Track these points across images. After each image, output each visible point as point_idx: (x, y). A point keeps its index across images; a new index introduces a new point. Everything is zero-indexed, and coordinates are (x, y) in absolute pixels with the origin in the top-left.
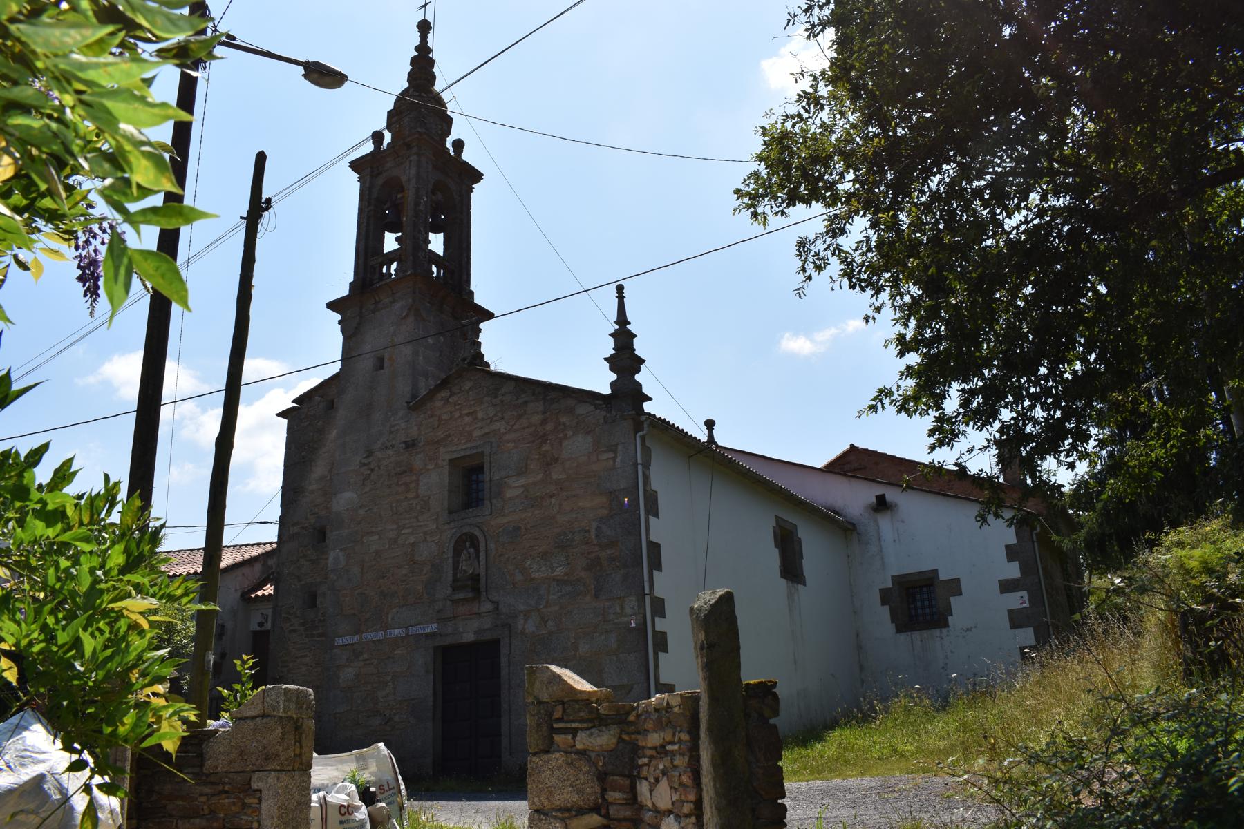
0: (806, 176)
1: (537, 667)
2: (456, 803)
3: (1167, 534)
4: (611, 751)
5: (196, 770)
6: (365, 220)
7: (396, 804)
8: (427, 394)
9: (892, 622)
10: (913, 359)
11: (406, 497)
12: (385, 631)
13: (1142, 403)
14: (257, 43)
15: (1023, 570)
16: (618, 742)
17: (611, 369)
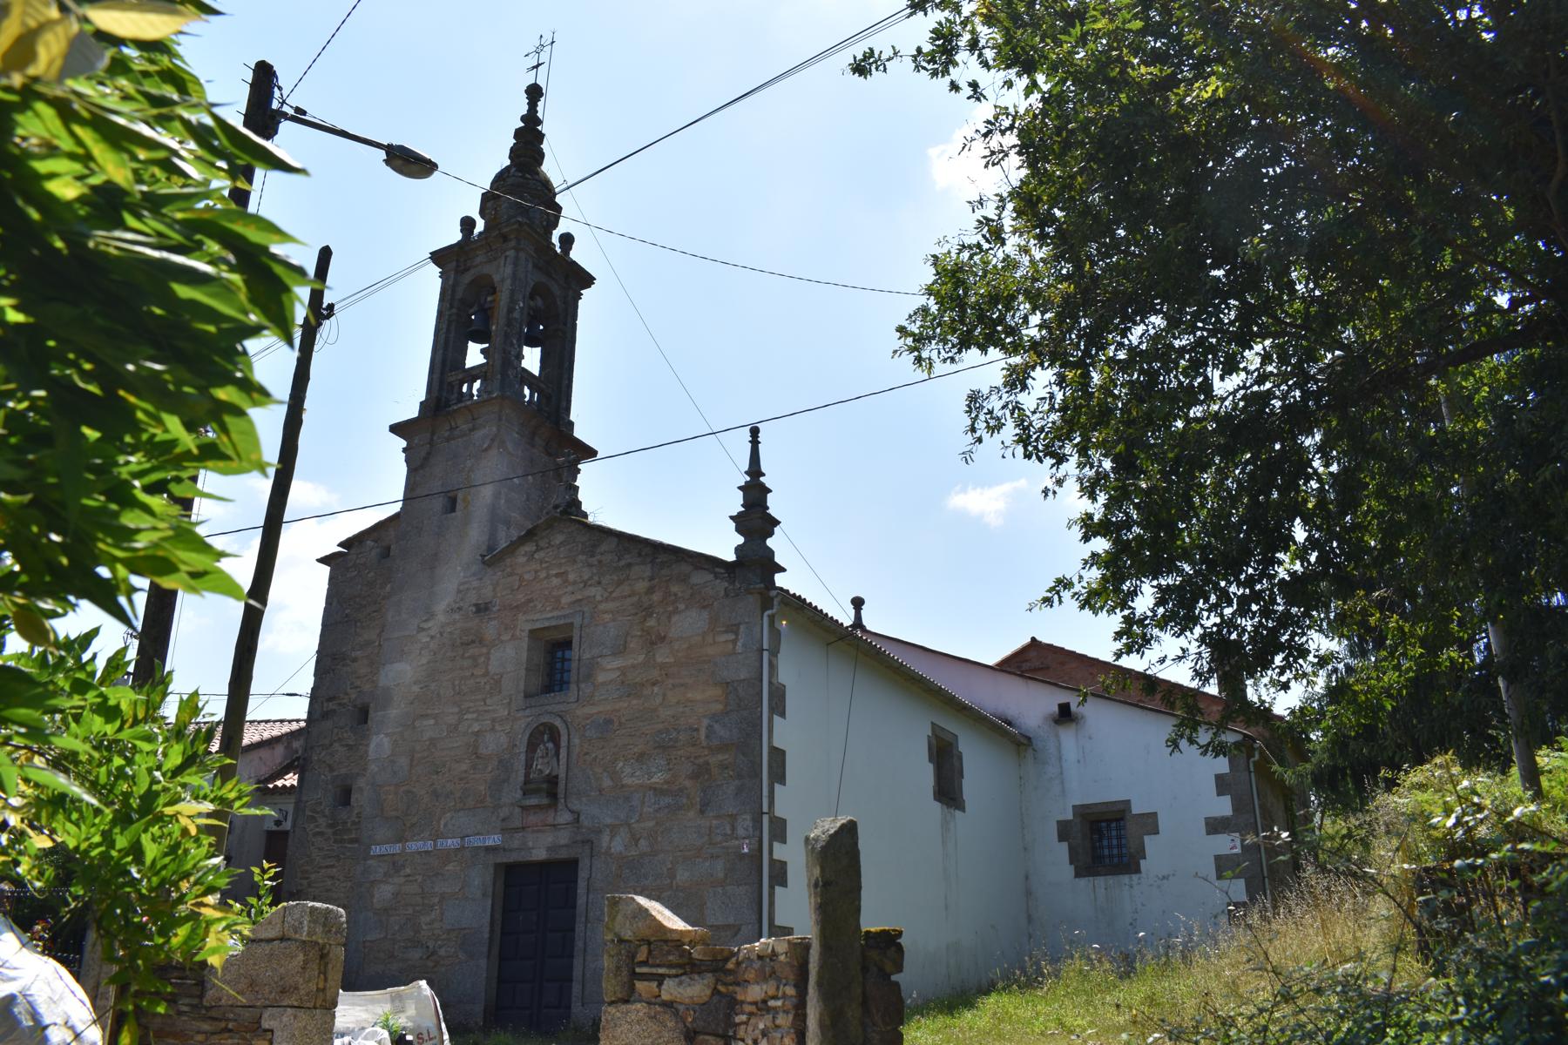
1: (620, 898)
3: (1407, 772)
4: (704, 1004)
5: (195, 1001)
6: (445, 326)
8: (508, 547)
9: (1071, 863)
10: (1101, 545)
11: (473, 674)
12: (434, 841)
13: (1373, 615)
14: (330, 121)
16: (713, 994)
17: (738, 530)
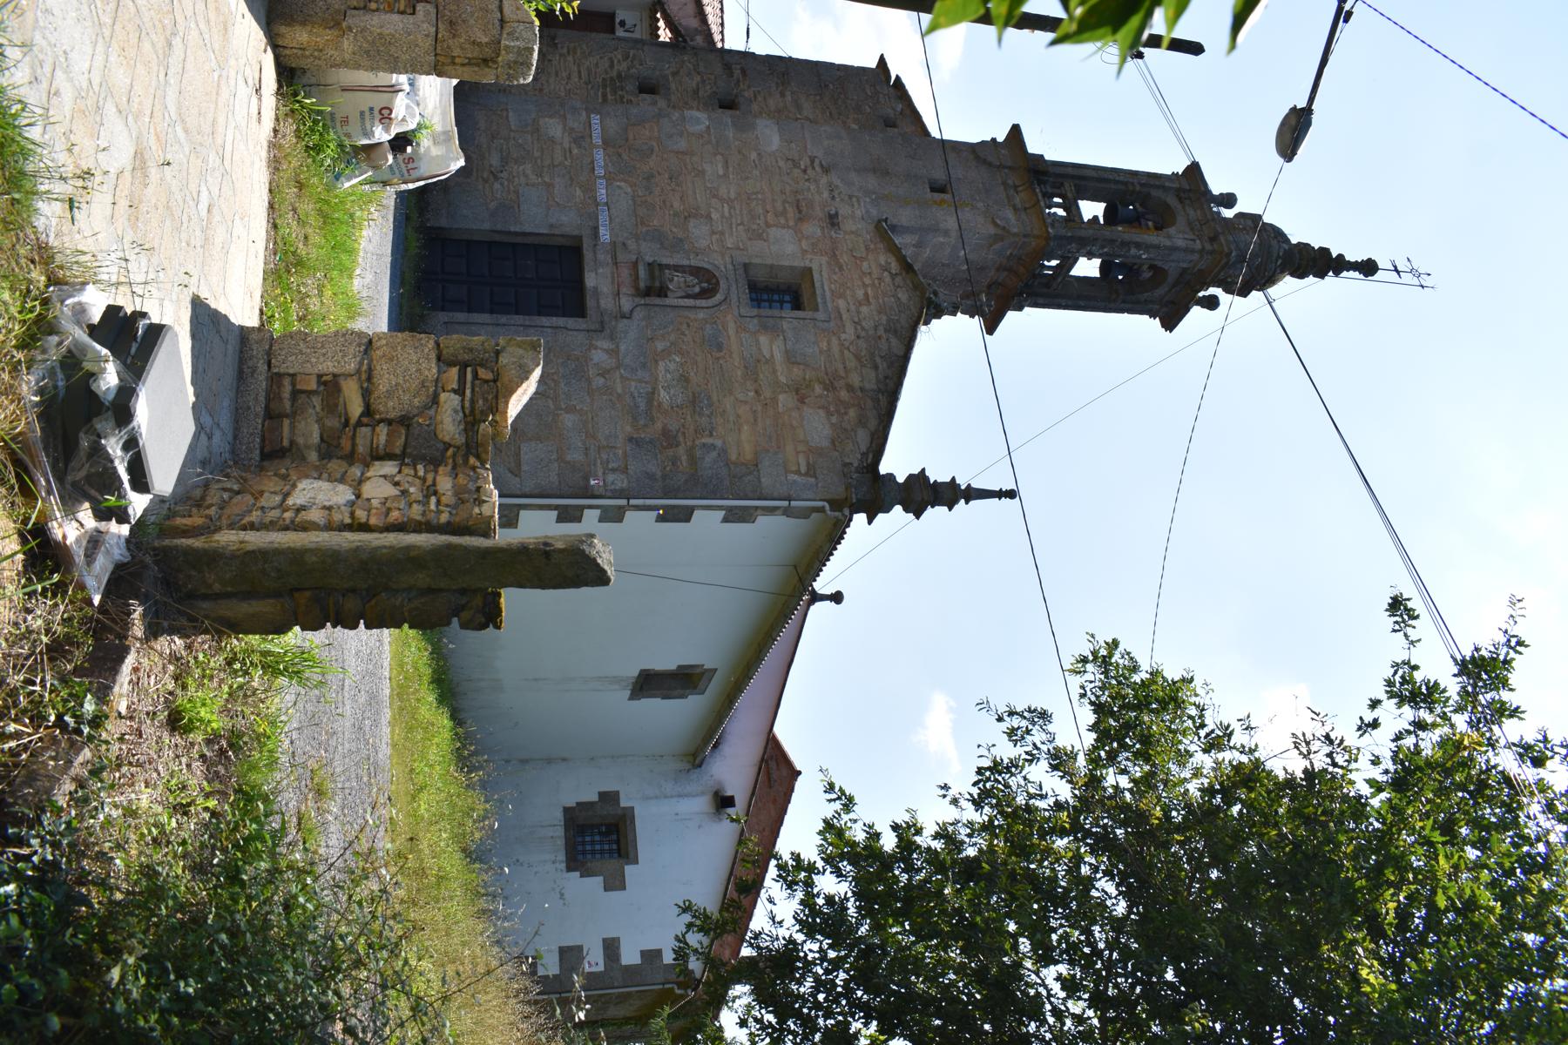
0: (1127, 727)
2: (389, 251)
6: (1122, 178)
7: (390, 177)
10: (889, 842)
12: (604, 177)
15: (629, 969)
16: (445, 443)
17: (911, 476)
